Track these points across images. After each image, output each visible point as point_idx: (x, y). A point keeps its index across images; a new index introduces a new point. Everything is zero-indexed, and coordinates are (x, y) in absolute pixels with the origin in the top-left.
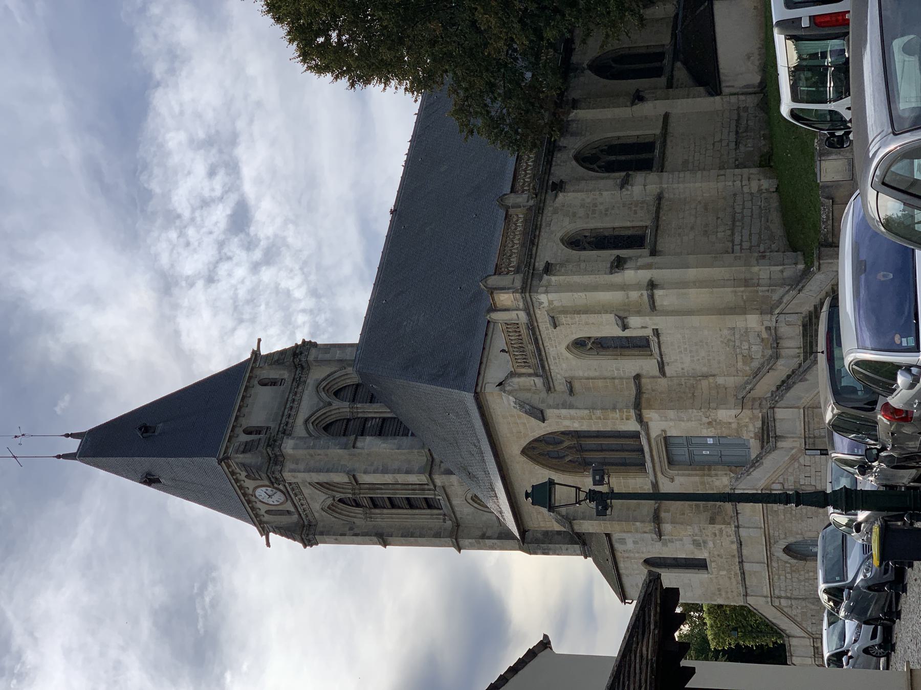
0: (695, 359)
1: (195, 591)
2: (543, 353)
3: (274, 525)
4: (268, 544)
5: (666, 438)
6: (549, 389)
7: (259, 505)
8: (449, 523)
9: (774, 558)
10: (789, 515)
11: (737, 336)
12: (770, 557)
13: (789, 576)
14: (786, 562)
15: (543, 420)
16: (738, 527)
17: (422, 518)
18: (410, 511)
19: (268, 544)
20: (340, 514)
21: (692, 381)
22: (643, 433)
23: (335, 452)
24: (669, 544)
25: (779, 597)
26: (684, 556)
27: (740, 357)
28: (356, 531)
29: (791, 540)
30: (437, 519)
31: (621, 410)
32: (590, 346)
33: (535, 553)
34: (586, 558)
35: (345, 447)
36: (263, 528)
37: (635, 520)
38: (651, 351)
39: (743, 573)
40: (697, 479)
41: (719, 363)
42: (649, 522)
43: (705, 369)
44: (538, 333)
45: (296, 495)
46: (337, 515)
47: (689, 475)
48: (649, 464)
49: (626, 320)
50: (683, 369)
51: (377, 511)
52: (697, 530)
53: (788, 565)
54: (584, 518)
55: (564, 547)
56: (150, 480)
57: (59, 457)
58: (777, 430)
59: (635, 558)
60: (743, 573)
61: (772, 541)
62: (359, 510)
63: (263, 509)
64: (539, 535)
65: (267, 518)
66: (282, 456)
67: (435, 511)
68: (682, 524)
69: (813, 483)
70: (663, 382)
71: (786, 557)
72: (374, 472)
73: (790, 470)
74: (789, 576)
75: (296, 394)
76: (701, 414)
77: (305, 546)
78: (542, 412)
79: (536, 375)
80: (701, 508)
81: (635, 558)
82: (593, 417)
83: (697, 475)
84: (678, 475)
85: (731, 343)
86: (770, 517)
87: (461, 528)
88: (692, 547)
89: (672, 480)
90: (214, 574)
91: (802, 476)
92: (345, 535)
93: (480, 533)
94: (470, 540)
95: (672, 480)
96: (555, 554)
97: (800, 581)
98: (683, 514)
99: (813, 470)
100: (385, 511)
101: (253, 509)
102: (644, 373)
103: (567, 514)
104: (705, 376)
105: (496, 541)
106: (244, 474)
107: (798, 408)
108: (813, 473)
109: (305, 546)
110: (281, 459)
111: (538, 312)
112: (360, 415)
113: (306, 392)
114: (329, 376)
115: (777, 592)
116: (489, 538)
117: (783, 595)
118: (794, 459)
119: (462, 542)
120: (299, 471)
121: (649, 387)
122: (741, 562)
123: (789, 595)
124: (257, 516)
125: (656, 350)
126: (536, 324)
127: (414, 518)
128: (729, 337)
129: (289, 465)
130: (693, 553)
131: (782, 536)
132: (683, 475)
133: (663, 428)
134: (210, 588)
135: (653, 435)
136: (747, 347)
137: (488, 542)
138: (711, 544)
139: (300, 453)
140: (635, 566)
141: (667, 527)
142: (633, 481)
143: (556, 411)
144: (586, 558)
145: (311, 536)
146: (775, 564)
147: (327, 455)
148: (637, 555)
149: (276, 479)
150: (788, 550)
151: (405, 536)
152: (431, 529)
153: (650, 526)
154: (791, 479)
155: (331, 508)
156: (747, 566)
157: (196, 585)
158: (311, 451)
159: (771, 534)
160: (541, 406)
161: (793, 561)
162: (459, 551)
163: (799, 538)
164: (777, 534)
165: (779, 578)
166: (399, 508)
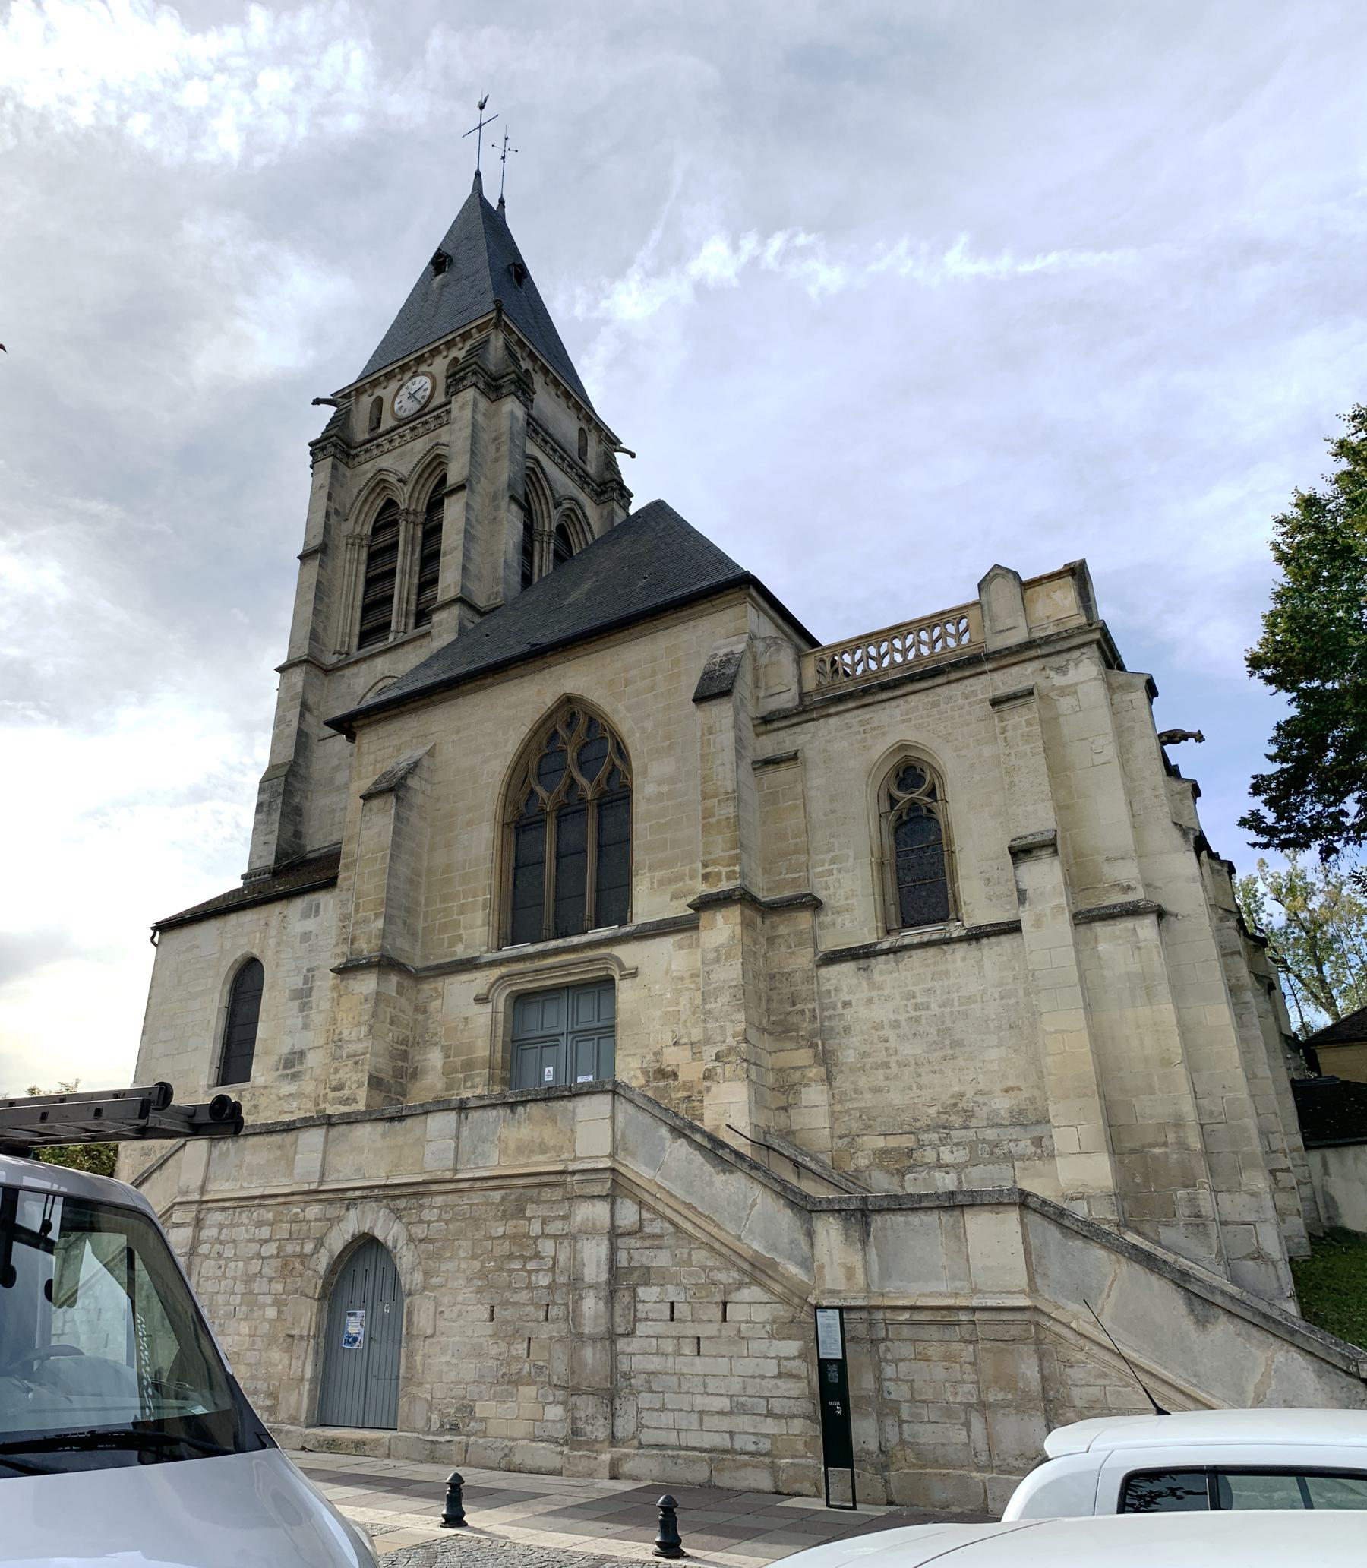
0: (887, 1032)
1: (43, 703)
2: (884, 696)
3: (353, 408)
4: (317, 402)
5: (609, 983)
6: (767, 721)
7: (394, 385)
8: (334, 659)
9: (334, 1211)
10: (505, 1248)
11: (991, 1134)
12: (345, 1198)
13: (271, 1249)
14: (320, 1243)
15: (700, 699)
16: (462, 1107)
17: (346, 620)
18: (359, 603)
19: (317, 402)
20: (366, 500)
21: (806, 1027)
22: (627, 929)
23: (503, 472)
24: (296, 1003)
25: (198, 1224)
26: (259, 1035)
27: (908, 1141)
28: (333, 519)
29: (405, 1258)
30: (343, 642)
31: (737, 859)
32: (904, 797)
33: (261, 791)
34: (244, 877)
35: (510, 486)
36: (346, 396)
37: (389, 919)
38: (899, 930)
39: (289, 1128)
40: (482, 1051)
41: (876, 1090)
42: (382, 948)
43: (849, 1056)
44: (953, 676)
45: (413, 429)
46: (364, 493)
47: (493, 1034)
48: (510, 951)
49: (1046, 853)
50: (846, 1004)
51: (364, 555)
52: (352, 1048)
53: (309, 1247)
54: (398, 817)
55: (273, 839)
56: (440, 262)
57: (478, 174)
58: (890, 1218)
59: (264, 939)
60: (289, 1128)
61: (402, 1203)
62: (368, 529)
63: (385, 393)
64: (297, 800)
65: (367, 401)
66: (498, 398)
67: (355, 641)
68: (374, 1015)
69: (642, 1329)
70: (803, 960)
71: (338, 1240)
72: (467, 519)
73: (700, 1256)
74: (271, 1249)
75: (570, 466)
76: (731, 1042)
77: (311, 444)
78: (726, 693)
79: (802, 695)
80: (400, 1063)
81: (264, 939)
82: (709, 803)
83: (493, 1052)
84: (495, 1012)
85: (956, 1120)
86: (497, 1195)
87: (322, 676)
88: (286, 1050)
89: (480, 1000)
90: (56, 723)
91: (672, 1293)
92: (330, 497)
93: (310, 702)
94: (301, 684)
95: (480, 1000)
96: (257, 823)
97: (249, 1280)
98: (392, 1023)
99: (704, 1331)
100: (363, 568)
101: (389, 376)
102: (826, 918)
103: (408, 788)
104: (826, 1059)
105: (295, 724)
106: (461, 354)
107: (1033, 1290)
108: (690, 1330)
109: (311, 444)
110: (493, 396)
111: (1030, 668)
112: (537, 545)
113: (571, 483)
114: (589, 524)
115: (218, 1217)
116: (302, 715)
117: (205, 1234)
118: (758, 1271)
119: (298, 676)
120: (474, 411)
121: (783, 930)
122: (328, 1122)
123: (204, 1249)
124: (375, 384)
125: (912, 936)
126: (987, 667)
127: (346, 607)
128: (981, 1113)
129: (483, 403)
130: (266, 1053)
131: (419, 1231)
132: (494, 1022)
133: (644, 971)
134: (42, 717)
135: (619, 951)
136: (947, 1157)
137: (294, 715)
138: (290, 1088)
139: (505, 424)
140: (243, 941)
141: (367, 984)
142: (479, 922)
143: (729, 721)
144: (244, 877)
145: (332, 450)
146: (314, 1211)
147: (497, 460)
148: (272, 942)
149: (463, 378)
150: (366, 1245)
151: (318, 587)
152: (325, 629)
153: (367, 947)
154: (662, 1259)
155: (380, 484)
156: (313, 1138)
157: (46, 705)
158: (505, 438)
159: (426, 1201)
160: (736, 694)
161: (322, 1262)
162: (279, 670)
163: (411, 1279)
164: (427, 1215)
165: (260, 1224)
166: (366, 592)
